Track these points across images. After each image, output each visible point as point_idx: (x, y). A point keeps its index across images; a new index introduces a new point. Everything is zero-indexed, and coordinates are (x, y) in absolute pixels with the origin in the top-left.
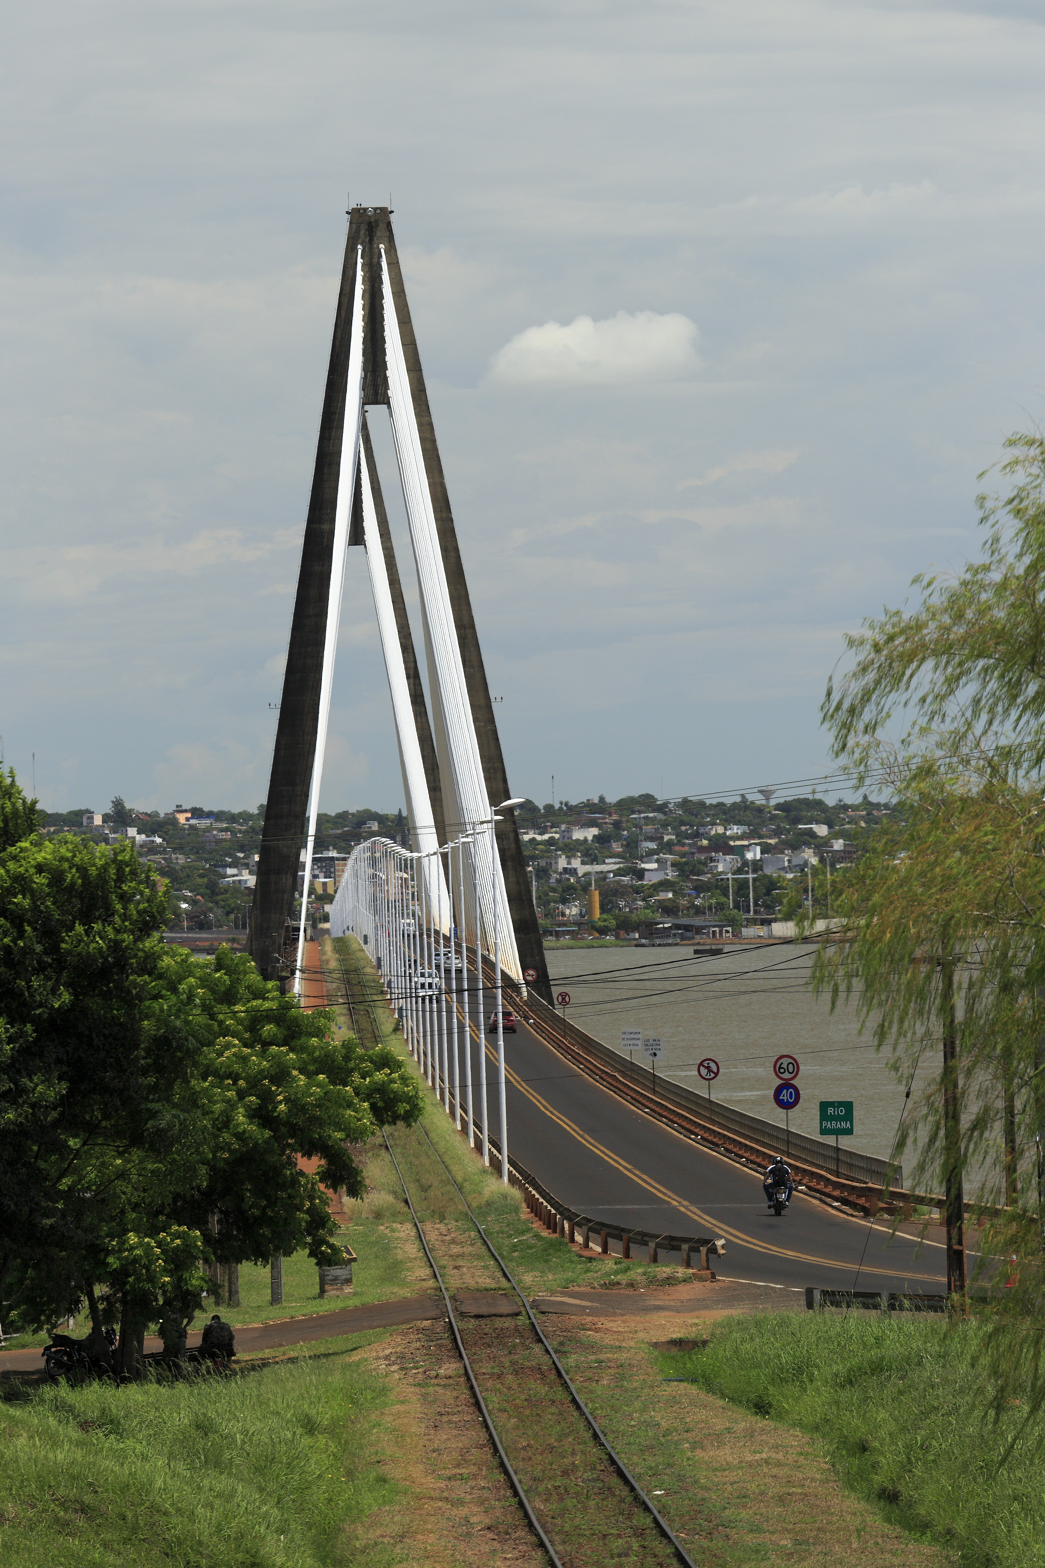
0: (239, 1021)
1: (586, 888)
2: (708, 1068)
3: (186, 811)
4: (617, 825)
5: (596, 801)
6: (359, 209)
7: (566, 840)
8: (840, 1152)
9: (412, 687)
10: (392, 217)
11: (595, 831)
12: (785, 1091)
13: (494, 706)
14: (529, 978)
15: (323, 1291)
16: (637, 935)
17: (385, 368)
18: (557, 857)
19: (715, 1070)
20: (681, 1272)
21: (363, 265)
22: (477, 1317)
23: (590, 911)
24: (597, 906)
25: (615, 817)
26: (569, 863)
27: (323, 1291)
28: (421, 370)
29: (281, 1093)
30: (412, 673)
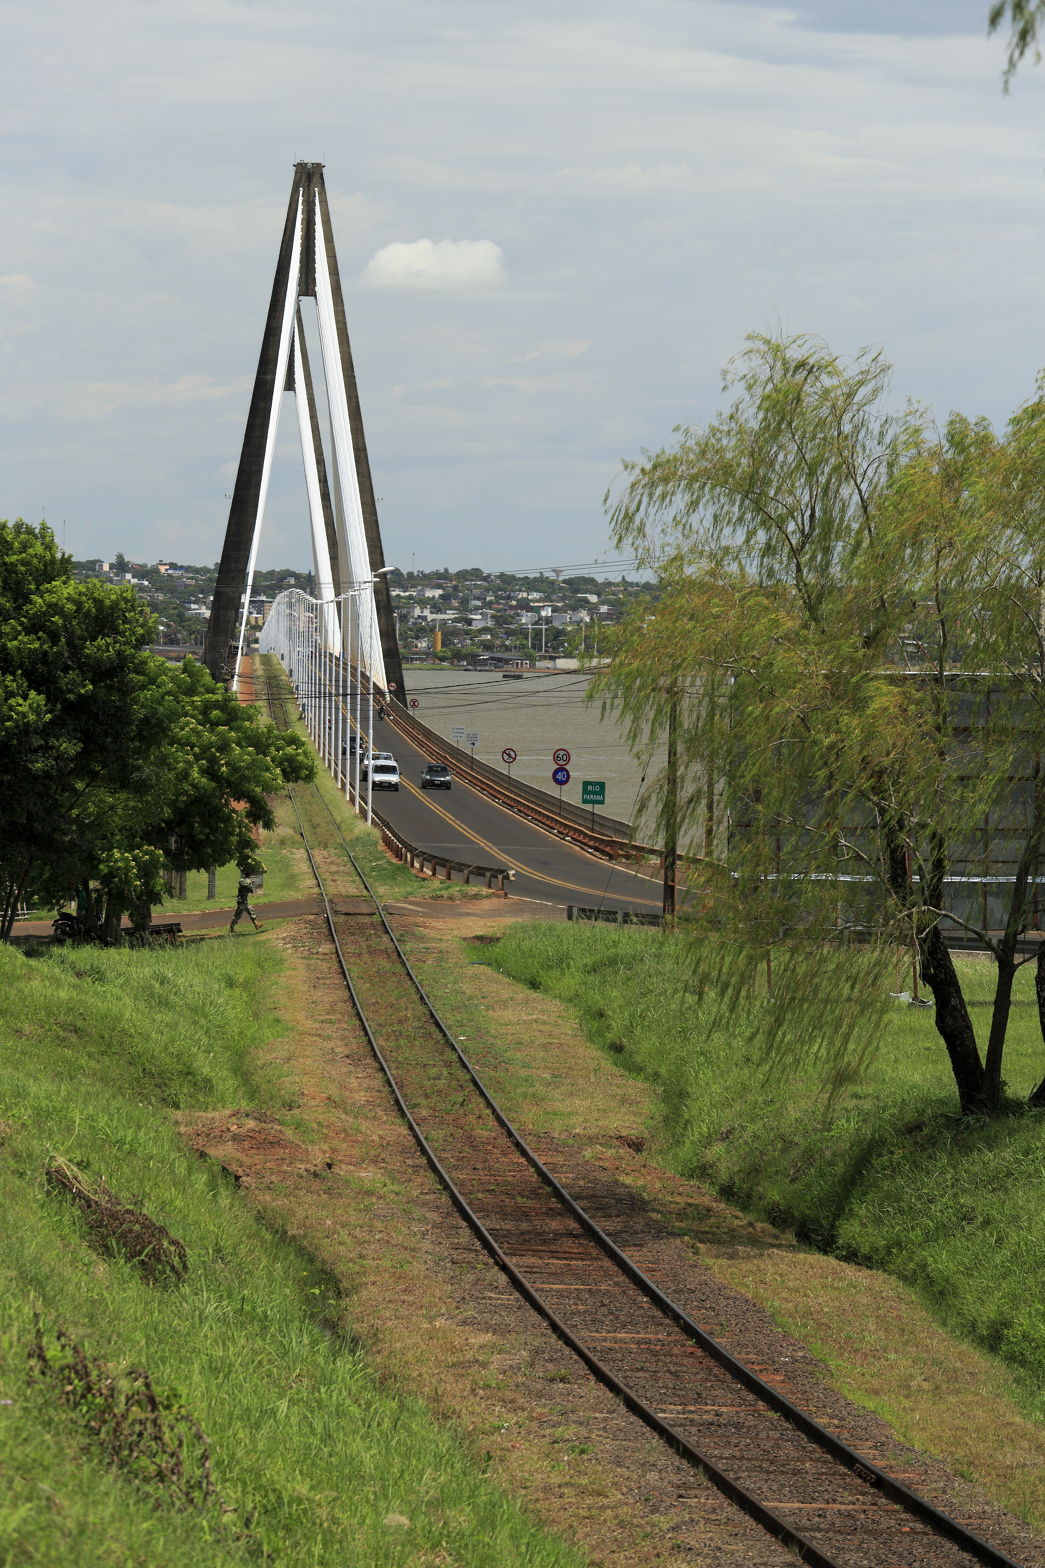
1: (432, 630)
2: (509, 755)
4: (455, 588)
10: (324, 170)
11: (440, 592)
13: (377, 504)
18: (414, 608)
20: (485, 891)
22: (346, 914)
23: (434, 645)
24: (439, 642)
25: (454, 583)
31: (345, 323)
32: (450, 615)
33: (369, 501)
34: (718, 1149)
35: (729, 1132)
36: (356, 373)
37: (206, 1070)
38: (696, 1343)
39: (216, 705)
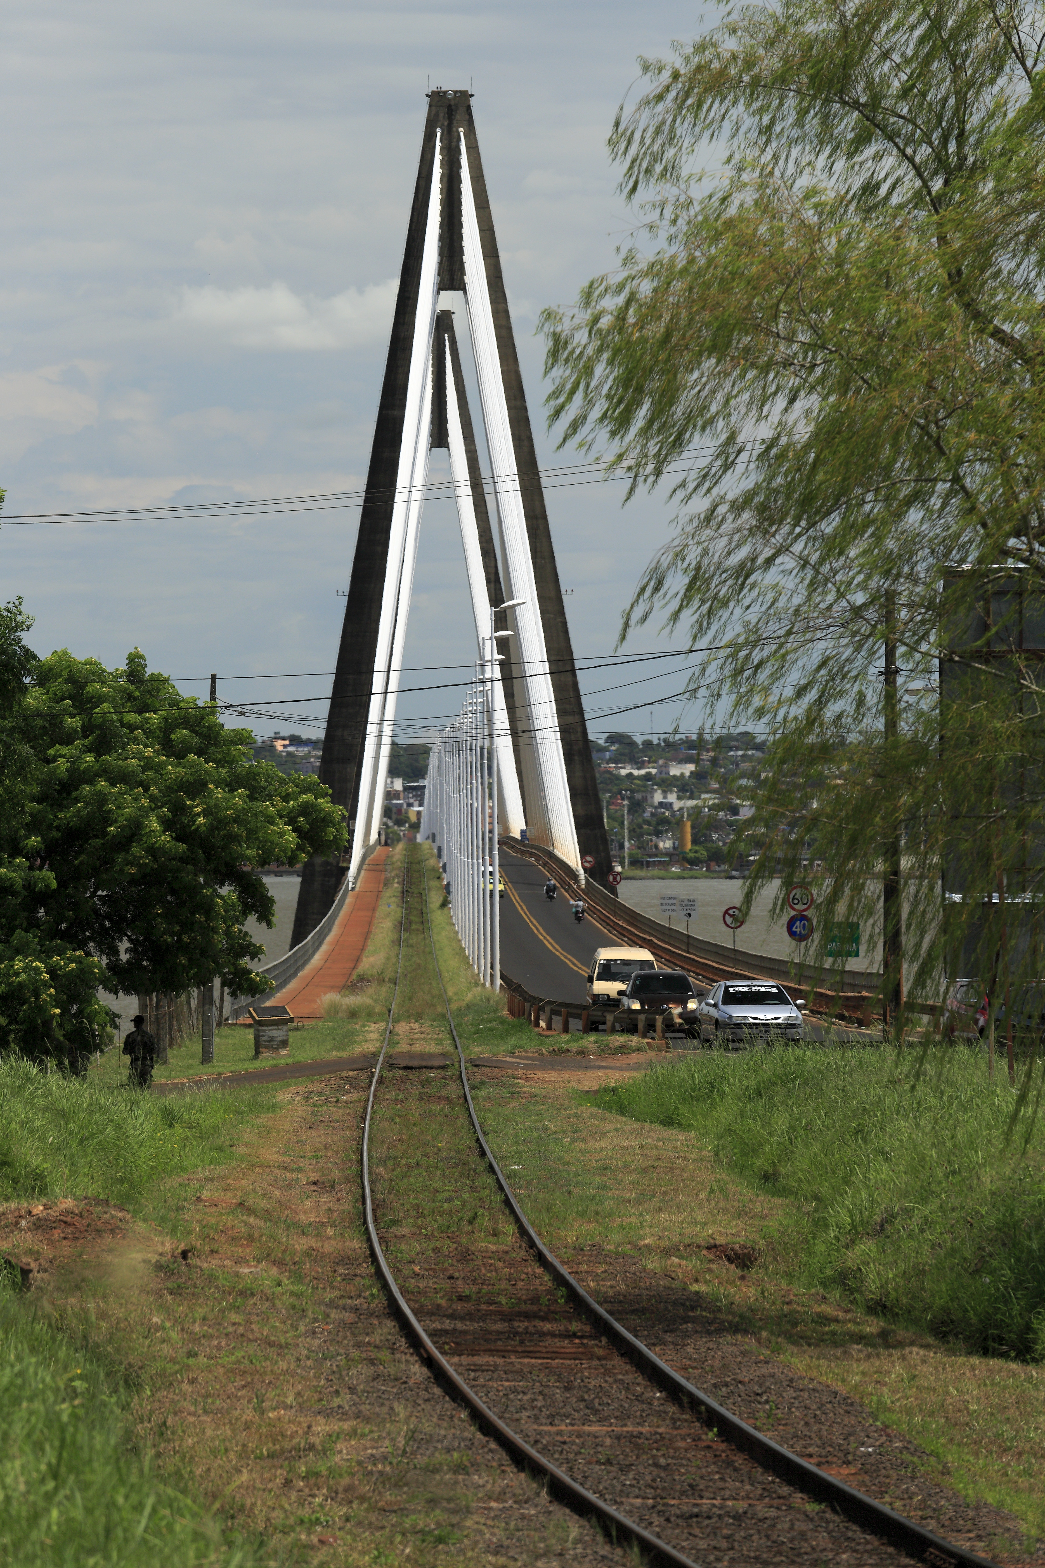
1: (680, 823)
3: (283, 738)
5: (694, 737)
6: (439, 92)
7: (664, 776)
10: (473, 101)
12: (798, 923)
13: (566, 599)
14: (587, 865)
15: (257, 1052)
17: (461, 253)
18: (653, 791)
21: (442, 149)
22: (406, 1068)
23: (682, 840)
24: (689, 837)
26: (665, 797)
27: (257, 1052)
30: (492, 577)
32: (710, 799)
37: (35, 1161)
38: (719, 1435)
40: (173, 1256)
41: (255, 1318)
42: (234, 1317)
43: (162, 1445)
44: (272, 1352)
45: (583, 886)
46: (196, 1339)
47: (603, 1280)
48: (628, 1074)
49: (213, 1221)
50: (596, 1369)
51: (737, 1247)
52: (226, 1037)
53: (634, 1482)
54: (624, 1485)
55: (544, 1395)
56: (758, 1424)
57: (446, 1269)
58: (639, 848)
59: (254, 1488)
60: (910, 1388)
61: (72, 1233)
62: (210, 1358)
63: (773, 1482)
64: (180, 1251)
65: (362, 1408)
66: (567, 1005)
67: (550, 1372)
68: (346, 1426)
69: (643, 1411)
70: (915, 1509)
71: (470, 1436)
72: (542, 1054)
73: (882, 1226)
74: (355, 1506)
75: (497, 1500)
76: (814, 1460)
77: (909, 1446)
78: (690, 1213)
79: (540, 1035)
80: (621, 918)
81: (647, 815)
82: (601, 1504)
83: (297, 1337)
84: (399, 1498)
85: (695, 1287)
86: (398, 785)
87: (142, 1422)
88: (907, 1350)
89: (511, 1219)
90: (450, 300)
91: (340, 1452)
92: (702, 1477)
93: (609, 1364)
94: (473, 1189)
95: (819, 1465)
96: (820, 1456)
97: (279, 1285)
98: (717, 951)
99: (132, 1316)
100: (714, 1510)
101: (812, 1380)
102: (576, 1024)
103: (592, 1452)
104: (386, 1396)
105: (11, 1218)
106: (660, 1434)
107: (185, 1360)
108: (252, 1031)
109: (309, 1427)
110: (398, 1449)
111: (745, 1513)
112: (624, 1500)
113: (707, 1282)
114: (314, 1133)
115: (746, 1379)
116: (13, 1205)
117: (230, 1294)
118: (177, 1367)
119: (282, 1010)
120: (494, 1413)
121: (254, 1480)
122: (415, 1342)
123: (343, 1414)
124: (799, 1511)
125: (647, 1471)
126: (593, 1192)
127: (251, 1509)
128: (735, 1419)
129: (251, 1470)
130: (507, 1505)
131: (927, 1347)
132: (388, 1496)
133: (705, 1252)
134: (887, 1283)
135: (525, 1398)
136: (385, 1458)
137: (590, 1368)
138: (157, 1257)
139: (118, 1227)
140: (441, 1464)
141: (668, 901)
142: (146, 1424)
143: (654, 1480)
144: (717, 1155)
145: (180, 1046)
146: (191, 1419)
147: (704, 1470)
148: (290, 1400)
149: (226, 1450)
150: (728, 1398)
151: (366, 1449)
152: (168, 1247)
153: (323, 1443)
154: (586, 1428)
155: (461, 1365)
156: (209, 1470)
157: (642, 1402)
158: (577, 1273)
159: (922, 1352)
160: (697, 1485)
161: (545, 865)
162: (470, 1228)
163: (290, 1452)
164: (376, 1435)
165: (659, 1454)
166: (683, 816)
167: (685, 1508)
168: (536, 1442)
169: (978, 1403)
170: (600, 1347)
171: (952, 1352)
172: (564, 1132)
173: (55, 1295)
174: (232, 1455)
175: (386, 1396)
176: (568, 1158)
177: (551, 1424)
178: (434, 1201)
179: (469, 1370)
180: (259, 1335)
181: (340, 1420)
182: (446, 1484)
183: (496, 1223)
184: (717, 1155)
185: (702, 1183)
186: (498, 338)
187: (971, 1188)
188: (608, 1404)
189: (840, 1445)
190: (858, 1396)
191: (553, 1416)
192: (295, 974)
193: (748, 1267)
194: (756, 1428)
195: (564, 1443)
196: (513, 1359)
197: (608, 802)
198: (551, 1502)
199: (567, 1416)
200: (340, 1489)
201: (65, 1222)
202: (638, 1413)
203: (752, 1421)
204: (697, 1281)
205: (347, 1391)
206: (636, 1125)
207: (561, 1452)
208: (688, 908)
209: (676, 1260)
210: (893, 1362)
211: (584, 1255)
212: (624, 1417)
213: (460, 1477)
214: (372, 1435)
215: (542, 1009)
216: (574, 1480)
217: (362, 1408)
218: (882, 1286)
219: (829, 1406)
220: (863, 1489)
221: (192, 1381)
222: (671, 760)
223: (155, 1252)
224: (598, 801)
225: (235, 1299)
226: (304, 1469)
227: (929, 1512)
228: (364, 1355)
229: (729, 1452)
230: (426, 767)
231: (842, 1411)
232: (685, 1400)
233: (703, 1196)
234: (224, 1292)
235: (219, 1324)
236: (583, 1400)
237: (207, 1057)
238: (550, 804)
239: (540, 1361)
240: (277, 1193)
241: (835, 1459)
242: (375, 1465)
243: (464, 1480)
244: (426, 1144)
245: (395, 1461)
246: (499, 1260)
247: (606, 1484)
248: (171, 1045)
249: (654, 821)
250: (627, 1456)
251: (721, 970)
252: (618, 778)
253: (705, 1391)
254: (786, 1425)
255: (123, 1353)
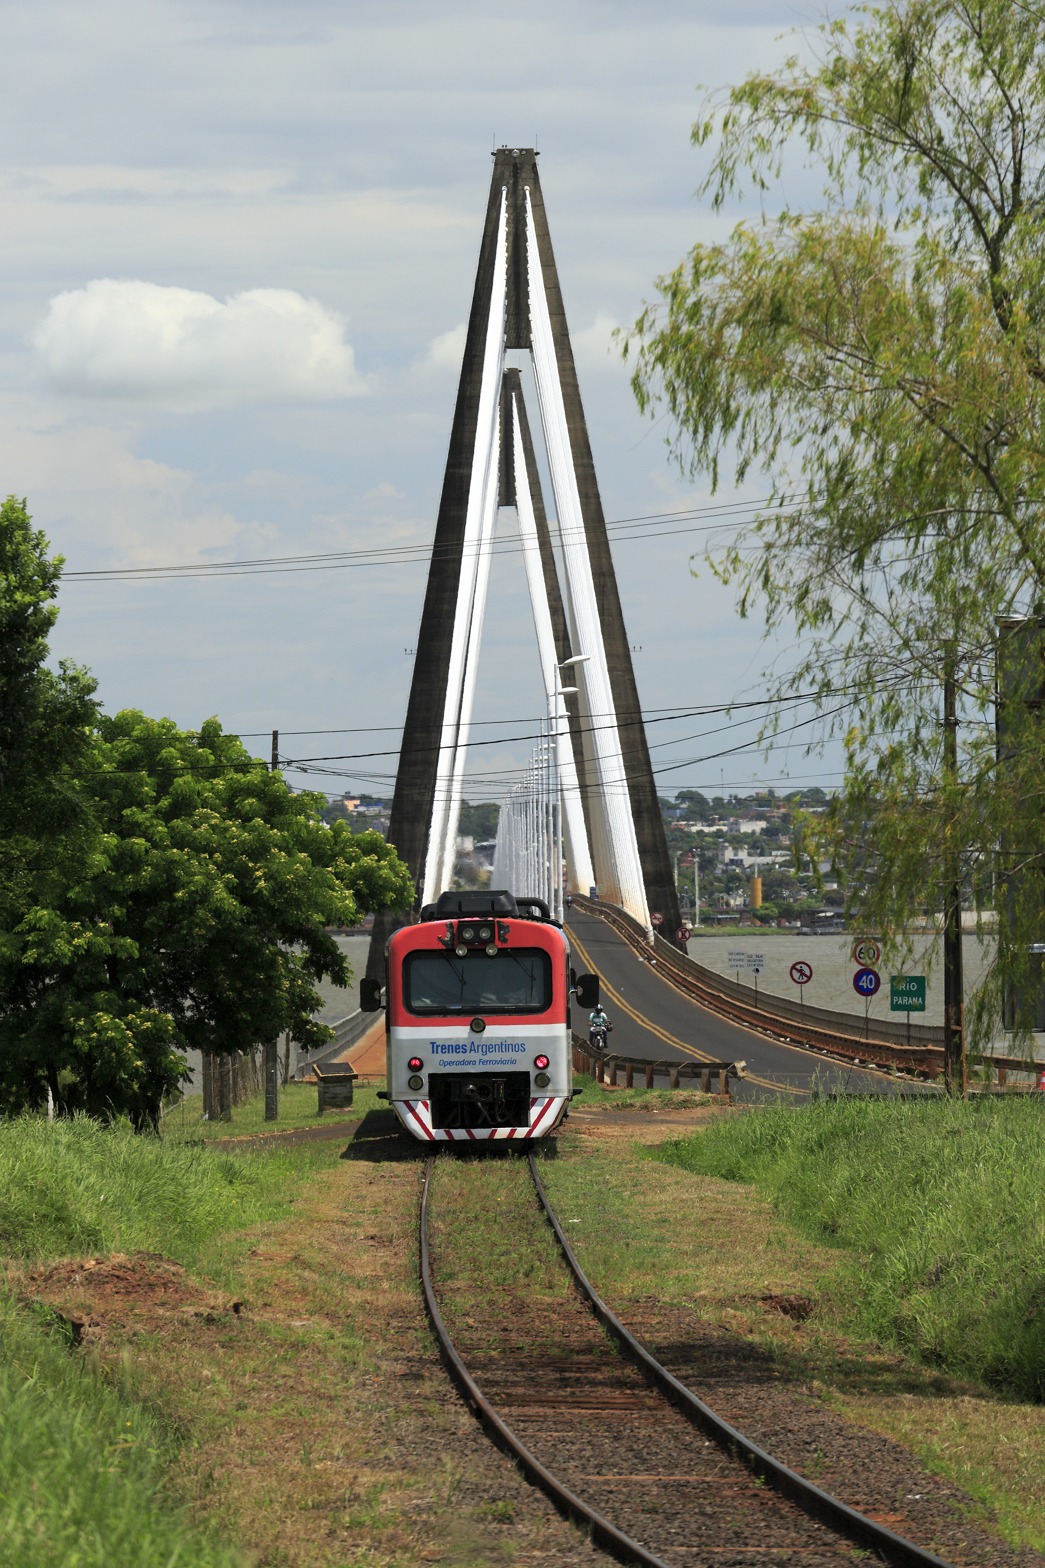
0: (217, 794)
1: (749, 879)
2: (801, 971)
3: (353, 798)
4: (785, 818)
6: (504, 151)
7: (734, 833)
8: (912, 1029)
9: (561, 649)
10: (538, 160)
11: (763, 824)
13: (634, 657)
15: (321, 1109)
16: (799, 924)
19: (808, 973)
20: (699, 1095)
21: (507, 207)
23: (753, 897)
25: (783, 810)
26: (736, 855)
28: (564, 314)
29: (260, 868)
30: (561, 635)
31: (576, 386)
32: (778, 857)
33: (621, 651)
34: (921, 1297)
35: (940, 1271)
36: (596, 462)
38: (765, 1483)
39: (249, 791)
40: (225, 1309)
41: (305, 1370)
42: (284, 1369)
43: (208, 1497)
44: (322, 1404)
45: (652, 944)
46: (246, 1392)
47: (658, 1331)
48: (691, 1128)
49: (267, 1274)
50: (646, 1419)
51: (792, 1298)
52: (292, 1094)
53: (679, 1530)
54: (669, 1533)
55: (593, 1445)
56: (806, 1472)
57: (500, 1322)
58: (710, 905)
59: (298, 1539)
60: (962, 1436)
61: (125, 1288)
62: (260, 1410)
63: (819, 1529)
64: (231, 1304)
65: (409, 1458)
66: (631, 1060)
67: (600, 1422)
68: (392, 1477)
69: (691, 1460)
70: (961, 1555)
71: (516, 1486)
72: (606, 1109)
73: (937, 1276)
74: (397, 1555)
75: (541, 1549)
76: (860, 1508)
77: (957, 1493)
78: (747, 1265)
79: (604, 1090)
80: (690, 974)
81: (718, 872)
82: (644, 1552)
83: (348, 1389)
84: (442, 1547)
85: (750, 1338)
86: (469, 844)
87: (189, 1474)
88: (960, 1398)
89: (567, 1272)
90: (517, 358)
91: (385, 1502)
92: (747, 1525)
93: (660, 1414)
94: (530, 1243)
95: (865, 1512)
96: (867, 1504)
97: (332, 1338)
98: (786, 1006)
99: (184, 1369)
100: (759, 1557)
101: (861, 1428)
102: (640, 1079)
103: (638, 1500)
104: (434, 1447)
105: (63, 1273)
106: (708, 1483)
107: (235, 1413)
108: (316, 1088)
109: (355, 1478)
110: (442, 1498)
111: (789, 1560)
112: (668, 1548)
113: (761, 1333)
114: (374, 1188)
115: (796, 1428)
116: (66, 1260)
117: (282, 1347)
118: (226, 1420)
119: (346, 1067)
120: (542, 1464)
121: (298, 1531)
122: (465, 1393)
123: (390, 1465)
124: (843, 1557)
125: (693, 1519)
126: (651, 1245)
127: (294, 1560)
128: (784, 1468)
129: (296, 1521)
130: (550, 1554)
131: (981, 1396)
132: (431, 1546)
133: (760, 1303)
134: (942, 1333)
135: (574, 1448)
136: (430, 1508)
137: (640, 1418)
138: (209, 1311)
139: (171, 1282)
140: (485, 1513)
141: (735, 957)
142: (192, 1476)
143: (699, 1528)
144: (776, 1206)
145: (245, 1104)
146: (238, 1471)
147: (749, 1518)
148: (337, 1451)
149: (271, 1501)
150: (778, 1447)
151: (411, 1499)
152: (220, 1301)
153: (368, 1494)
154: (634, 1477)
155: (511, 1416)
156: (253, 1521)
157: (691, 1451)
158: (631, 1324)
159: (974, 1401)
160: (742, 1533)
161: (614, 922)
162: (526, 1281)
163: (335, 1502)
164: (421, 1486)
165: (706, 1502)
166: (753, 873)
167: (729, 1556)
168: (583, 1491)
169: (1028, 1451)
170: (650, 1397)
171: (1004, 1400)
172: (625, 1186)
173: (107, 1349)
174: (277, 1506)
175: (434, 1447)
176: (627, 1211)
177: (598, 1473)
178: (491, 1254)
179: (518, 1421)
180: (309, 1388)
181: (386, 1471)
182: (490, 1534)
183: (552, 1275)
184: (776, 1206)
185: (760, 1235)
186: (565, 396)
187: (1025, 1237)
188: (656, 1453)
189: (887, 1492)
190: (908, 1444)
191: (601, 1466)
192: (364, 1031)
193: (803, 1318)
194: (803, 1476)
195: (611, 1492)
196: (563, 1409)
197: (679, 860)
198: (594, 1550)
199: (615, 1465)
200: (384, 1539)
201: (118, 1277)
202: (686, 1463)
203: (800, 1469)
204: (751, 1331)
205: (395, 1442)
206: (695, 1178)
207: (607, 1501)
208: (756, 964)
209: (731, 1311)
210: (945, 1411)
211: (640, 1307)
212: (672, 1466)
213: (505, 1527)
214: (417, 1486)
215: (606, 1064)
216: (619, 1528)
217: (409, 1458)
218: (937, 1336)
219: (878, 1454)
220: (909, 1536)
221: (241, 1434)
222: (742, 818)
223: (207, 1306)
224: (667, 858)
225: (286, 1351)
226: (347, 1519)
227: (974, 1558)
228: (414, 1407)
229: (776, 1500)
230: (496, 825)
231: (891, 1459)
232: (734, 1448)
233: (760, 1248)
234: (276, 1345)
235: (269, 1377)
236: (632, 1450)
237: (271, 1113)
238: (618, 861)
239: (590, 1411)
240: (334, 1248)
241: (882, 1507)
242: (419, 1514)
243: (508, 1529)
244: (486, 1197)
245: (440, 1511)
246: (554, 1312)
247: (651, 1532)
248: (235, 1103)
249: (724, 878)
250: (673, 1504)
251: (788, 1025)
252: (689, 835)
253: (755, 1440)
254: (833, 1473)
255: (172, 1406)
